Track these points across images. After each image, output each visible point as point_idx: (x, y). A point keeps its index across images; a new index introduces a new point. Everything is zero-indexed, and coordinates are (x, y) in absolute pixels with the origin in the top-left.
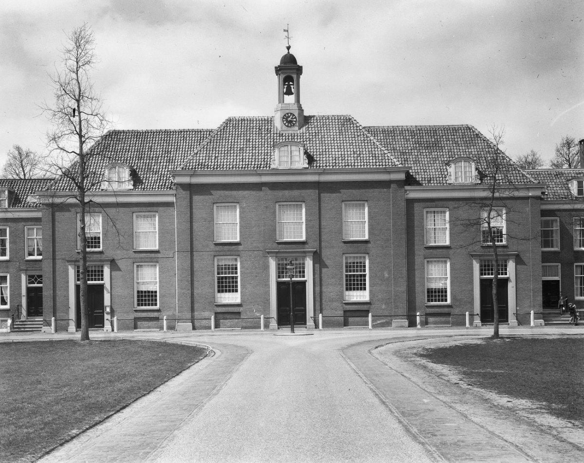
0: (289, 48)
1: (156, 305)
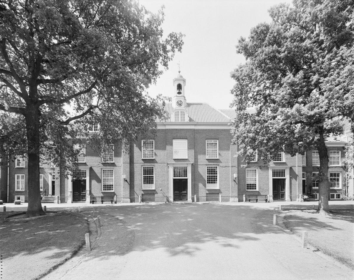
0: (179, 72)
1: (113, 190)
